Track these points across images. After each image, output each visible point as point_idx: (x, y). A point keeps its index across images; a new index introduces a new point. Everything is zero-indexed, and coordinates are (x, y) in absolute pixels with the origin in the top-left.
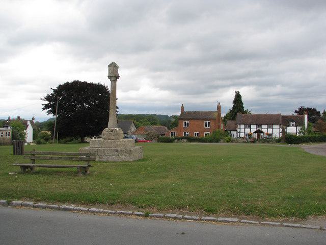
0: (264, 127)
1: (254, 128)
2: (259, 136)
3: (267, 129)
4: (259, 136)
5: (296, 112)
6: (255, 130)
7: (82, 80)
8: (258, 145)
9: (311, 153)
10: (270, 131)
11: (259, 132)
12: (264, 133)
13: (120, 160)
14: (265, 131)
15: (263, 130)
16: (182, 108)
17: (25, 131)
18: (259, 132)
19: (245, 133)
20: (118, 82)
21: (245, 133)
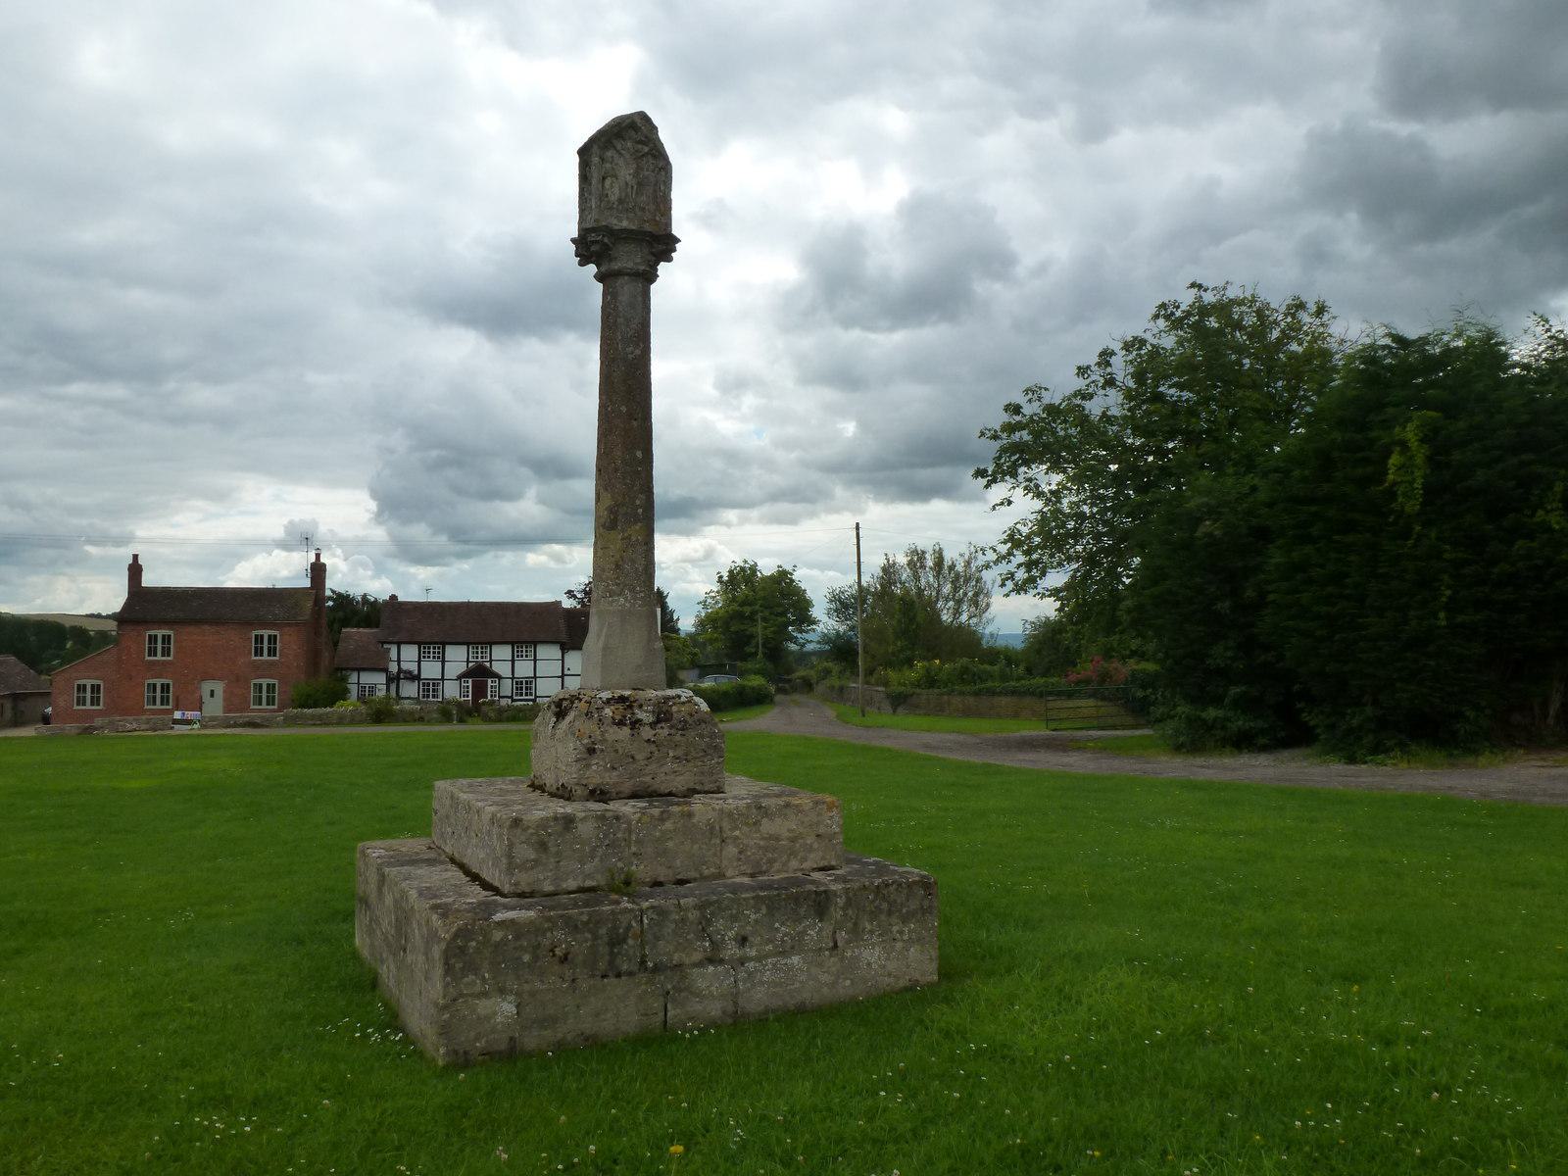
0: (502, 652)
1: (458, 658)
2: (480, 690)
3: (513, 661)
4: (480, 690)
5: (570, 594)
6: (462, 668)
7: (586, 140)
8: (475, 728)
9: (1091, 702)
10: (524, 669)
11: (479, 674)
12: (500, 678)
13: (846, 988)
14: (502, 668)
15: (497, 667)
16: (135, 570)
17: (682, 635)
18: (479, 674)
19: (513, 678)
20: (671, 285)
21: (513, 678)
